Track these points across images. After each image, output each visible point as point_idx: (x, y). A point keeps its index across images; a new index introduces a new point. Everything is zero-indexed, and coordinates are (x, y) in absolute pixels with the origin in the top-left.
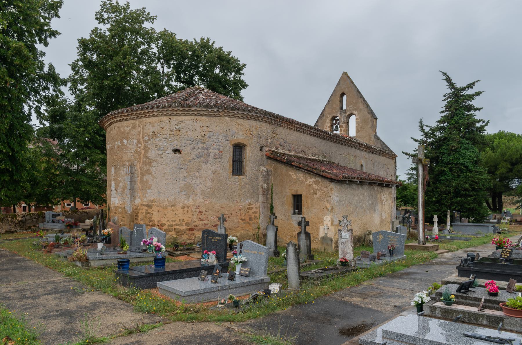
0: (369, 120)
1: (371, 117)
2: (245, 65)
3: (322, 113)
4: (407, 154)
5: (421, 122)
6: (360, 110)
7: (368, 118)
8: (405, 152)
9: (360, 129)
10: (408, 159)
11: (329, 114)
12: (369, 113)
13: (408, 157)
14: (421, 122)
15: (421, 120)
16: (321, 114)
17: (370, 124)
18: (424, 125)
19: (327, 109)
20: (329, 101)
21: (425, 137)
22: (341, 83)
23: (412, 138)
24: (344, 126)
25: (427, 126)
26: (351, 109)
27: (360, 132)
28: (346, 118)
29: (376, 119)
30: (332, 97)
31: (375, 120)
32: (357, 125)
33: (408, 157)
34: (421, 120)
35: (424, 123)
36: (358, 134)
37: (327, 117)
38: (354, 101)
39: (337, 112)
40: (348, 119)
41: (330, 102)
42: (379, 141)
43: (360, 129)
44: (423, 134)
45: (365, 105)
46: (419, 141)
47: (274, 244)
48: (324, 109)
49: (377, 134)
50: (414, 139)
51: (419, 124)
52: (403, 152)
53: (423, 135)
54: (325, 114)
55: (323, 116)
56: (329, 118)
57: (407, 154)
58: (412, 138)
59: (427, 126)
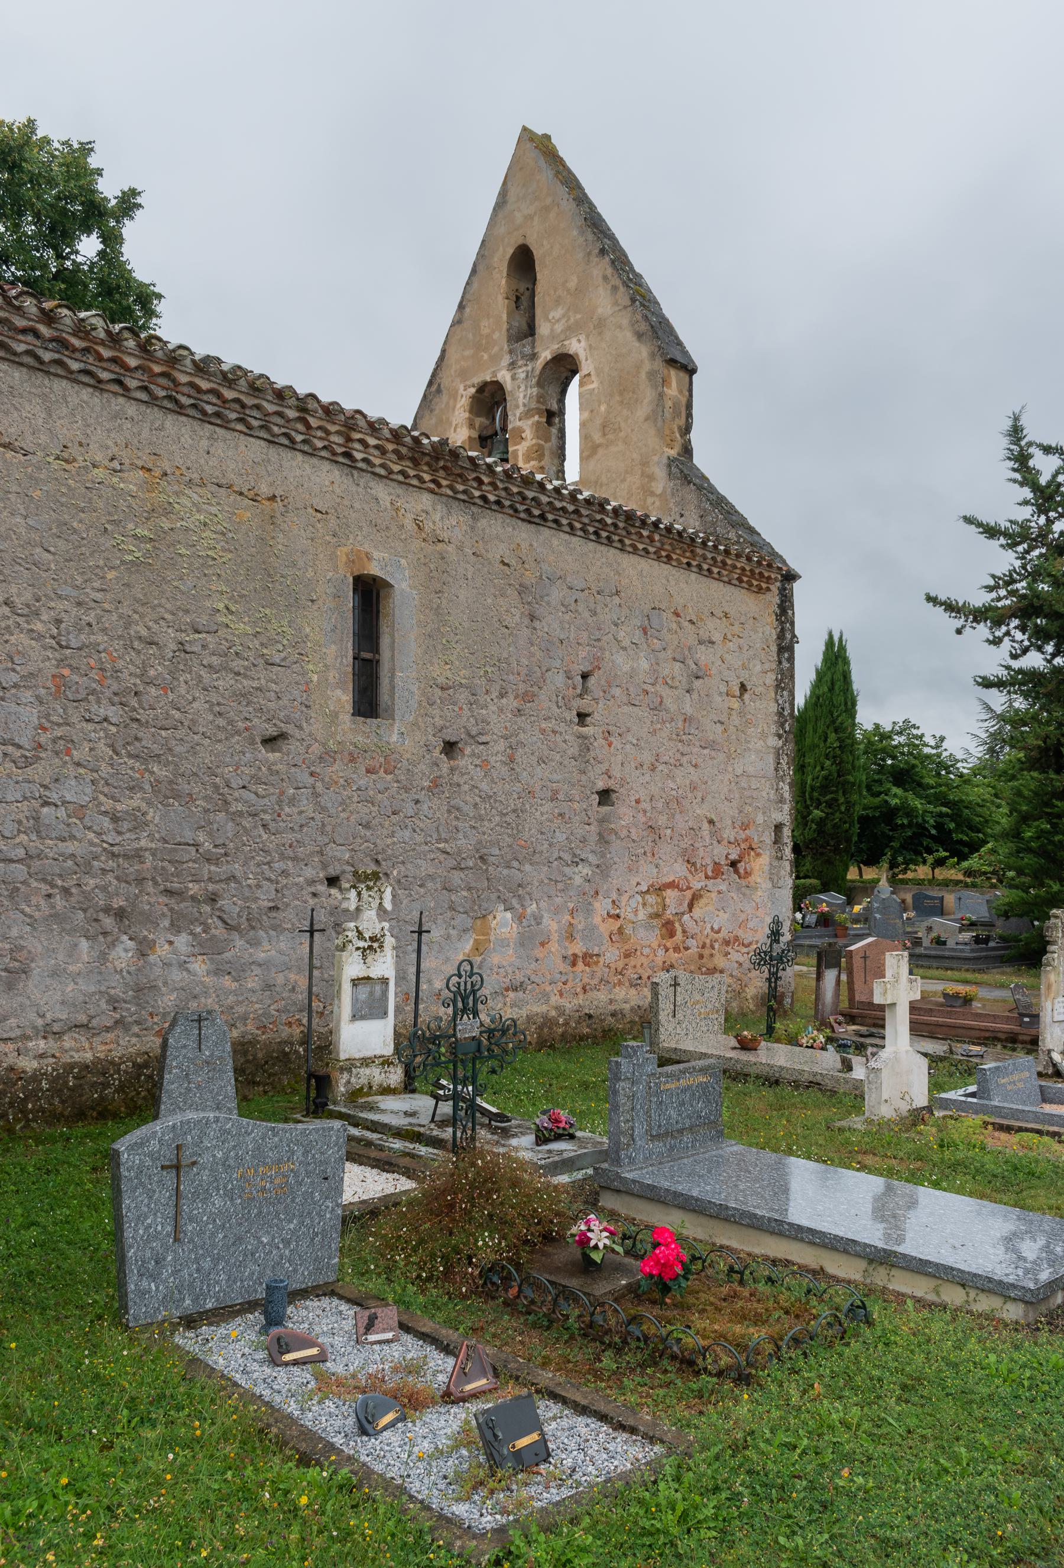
0: (643, 375)
1: (652, 356)
2: (134, 193)
3: (434, 375)
4: (951, 607)
5: (1016, 432)
6: (601, 325)
7: (638, 367)
8: (943, 597)
9: (597, 438)
10: (959, 632)
11: (463, 374)
12: (640, 336)
13: (959, 623)
14: (1016, 432)
15: (1016, 419)
16: (430, 383)
17: (648, 395)
18: (1030, 444)
19: (453, 355)
20: (461, 307)
21: (1042, 510)
22: (512, 197)
23: (969, 520)
24: (528, 434)
25: (1047, 450)
26: (559, 328)
27: (601, 452)
28: (539, 384)
29: (689, 370)
30: (475, 279)
31: (675, 376)
32: (586, 414)
33: (959, 623)
34: (1016, 419)
35: (1033, 433)
36: (592, 463)
37: (454, 396)
38: (572, 284)
39: (495, 359)
40: (553, 390)
41: (468, 310)
42: (690, 495)
43: (597, 438)
44: (1027, 493)
45: (622, 289)
46: (1006, 534)
47: (307, 960)
48: (443, 351)
49: (700, 460)
50: (980, 525)
51: (1005, 442)
52: (930, 599)
53: (1026, 503)
54: (445, 380)
55: (439, 391)
56: (465, 394)
57: (951, 607)
58: (969, 520)
59: (1047, 450)
